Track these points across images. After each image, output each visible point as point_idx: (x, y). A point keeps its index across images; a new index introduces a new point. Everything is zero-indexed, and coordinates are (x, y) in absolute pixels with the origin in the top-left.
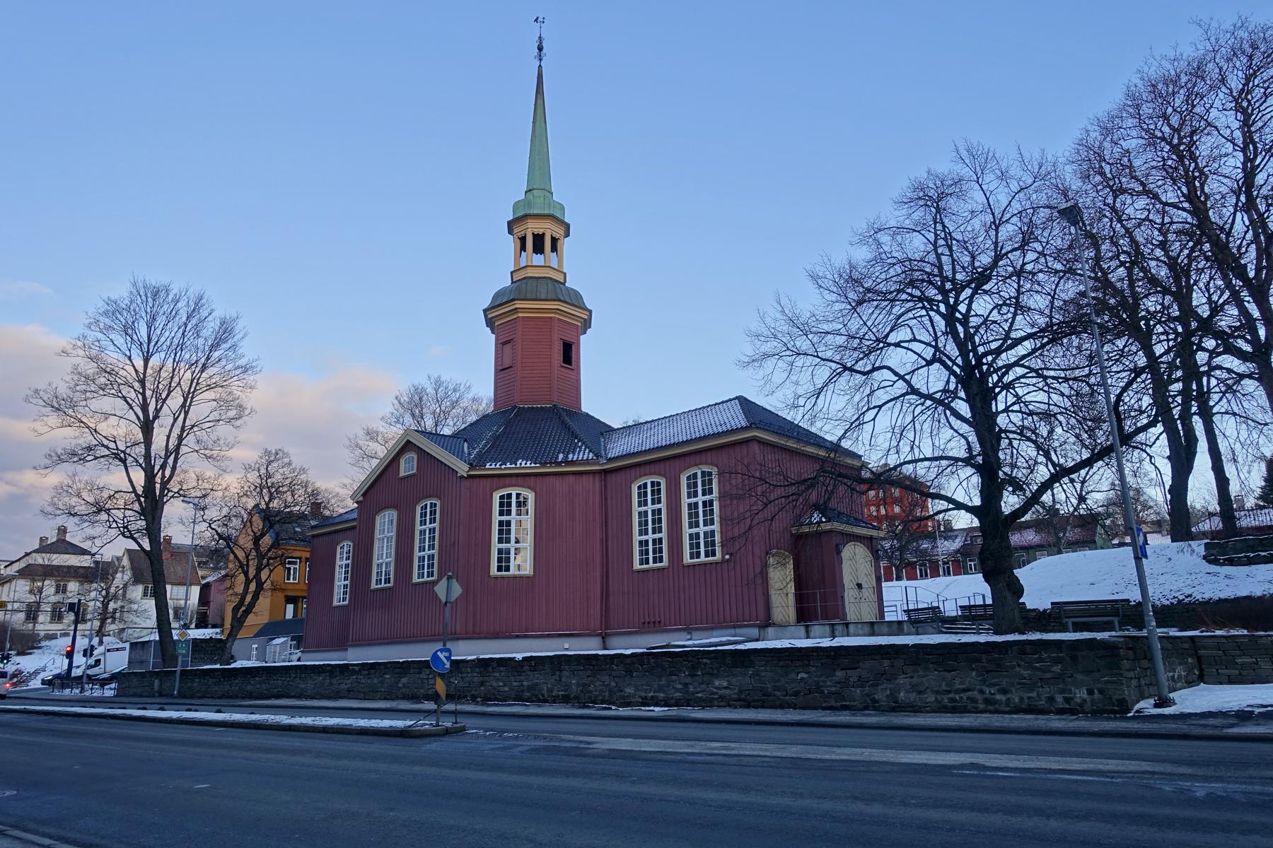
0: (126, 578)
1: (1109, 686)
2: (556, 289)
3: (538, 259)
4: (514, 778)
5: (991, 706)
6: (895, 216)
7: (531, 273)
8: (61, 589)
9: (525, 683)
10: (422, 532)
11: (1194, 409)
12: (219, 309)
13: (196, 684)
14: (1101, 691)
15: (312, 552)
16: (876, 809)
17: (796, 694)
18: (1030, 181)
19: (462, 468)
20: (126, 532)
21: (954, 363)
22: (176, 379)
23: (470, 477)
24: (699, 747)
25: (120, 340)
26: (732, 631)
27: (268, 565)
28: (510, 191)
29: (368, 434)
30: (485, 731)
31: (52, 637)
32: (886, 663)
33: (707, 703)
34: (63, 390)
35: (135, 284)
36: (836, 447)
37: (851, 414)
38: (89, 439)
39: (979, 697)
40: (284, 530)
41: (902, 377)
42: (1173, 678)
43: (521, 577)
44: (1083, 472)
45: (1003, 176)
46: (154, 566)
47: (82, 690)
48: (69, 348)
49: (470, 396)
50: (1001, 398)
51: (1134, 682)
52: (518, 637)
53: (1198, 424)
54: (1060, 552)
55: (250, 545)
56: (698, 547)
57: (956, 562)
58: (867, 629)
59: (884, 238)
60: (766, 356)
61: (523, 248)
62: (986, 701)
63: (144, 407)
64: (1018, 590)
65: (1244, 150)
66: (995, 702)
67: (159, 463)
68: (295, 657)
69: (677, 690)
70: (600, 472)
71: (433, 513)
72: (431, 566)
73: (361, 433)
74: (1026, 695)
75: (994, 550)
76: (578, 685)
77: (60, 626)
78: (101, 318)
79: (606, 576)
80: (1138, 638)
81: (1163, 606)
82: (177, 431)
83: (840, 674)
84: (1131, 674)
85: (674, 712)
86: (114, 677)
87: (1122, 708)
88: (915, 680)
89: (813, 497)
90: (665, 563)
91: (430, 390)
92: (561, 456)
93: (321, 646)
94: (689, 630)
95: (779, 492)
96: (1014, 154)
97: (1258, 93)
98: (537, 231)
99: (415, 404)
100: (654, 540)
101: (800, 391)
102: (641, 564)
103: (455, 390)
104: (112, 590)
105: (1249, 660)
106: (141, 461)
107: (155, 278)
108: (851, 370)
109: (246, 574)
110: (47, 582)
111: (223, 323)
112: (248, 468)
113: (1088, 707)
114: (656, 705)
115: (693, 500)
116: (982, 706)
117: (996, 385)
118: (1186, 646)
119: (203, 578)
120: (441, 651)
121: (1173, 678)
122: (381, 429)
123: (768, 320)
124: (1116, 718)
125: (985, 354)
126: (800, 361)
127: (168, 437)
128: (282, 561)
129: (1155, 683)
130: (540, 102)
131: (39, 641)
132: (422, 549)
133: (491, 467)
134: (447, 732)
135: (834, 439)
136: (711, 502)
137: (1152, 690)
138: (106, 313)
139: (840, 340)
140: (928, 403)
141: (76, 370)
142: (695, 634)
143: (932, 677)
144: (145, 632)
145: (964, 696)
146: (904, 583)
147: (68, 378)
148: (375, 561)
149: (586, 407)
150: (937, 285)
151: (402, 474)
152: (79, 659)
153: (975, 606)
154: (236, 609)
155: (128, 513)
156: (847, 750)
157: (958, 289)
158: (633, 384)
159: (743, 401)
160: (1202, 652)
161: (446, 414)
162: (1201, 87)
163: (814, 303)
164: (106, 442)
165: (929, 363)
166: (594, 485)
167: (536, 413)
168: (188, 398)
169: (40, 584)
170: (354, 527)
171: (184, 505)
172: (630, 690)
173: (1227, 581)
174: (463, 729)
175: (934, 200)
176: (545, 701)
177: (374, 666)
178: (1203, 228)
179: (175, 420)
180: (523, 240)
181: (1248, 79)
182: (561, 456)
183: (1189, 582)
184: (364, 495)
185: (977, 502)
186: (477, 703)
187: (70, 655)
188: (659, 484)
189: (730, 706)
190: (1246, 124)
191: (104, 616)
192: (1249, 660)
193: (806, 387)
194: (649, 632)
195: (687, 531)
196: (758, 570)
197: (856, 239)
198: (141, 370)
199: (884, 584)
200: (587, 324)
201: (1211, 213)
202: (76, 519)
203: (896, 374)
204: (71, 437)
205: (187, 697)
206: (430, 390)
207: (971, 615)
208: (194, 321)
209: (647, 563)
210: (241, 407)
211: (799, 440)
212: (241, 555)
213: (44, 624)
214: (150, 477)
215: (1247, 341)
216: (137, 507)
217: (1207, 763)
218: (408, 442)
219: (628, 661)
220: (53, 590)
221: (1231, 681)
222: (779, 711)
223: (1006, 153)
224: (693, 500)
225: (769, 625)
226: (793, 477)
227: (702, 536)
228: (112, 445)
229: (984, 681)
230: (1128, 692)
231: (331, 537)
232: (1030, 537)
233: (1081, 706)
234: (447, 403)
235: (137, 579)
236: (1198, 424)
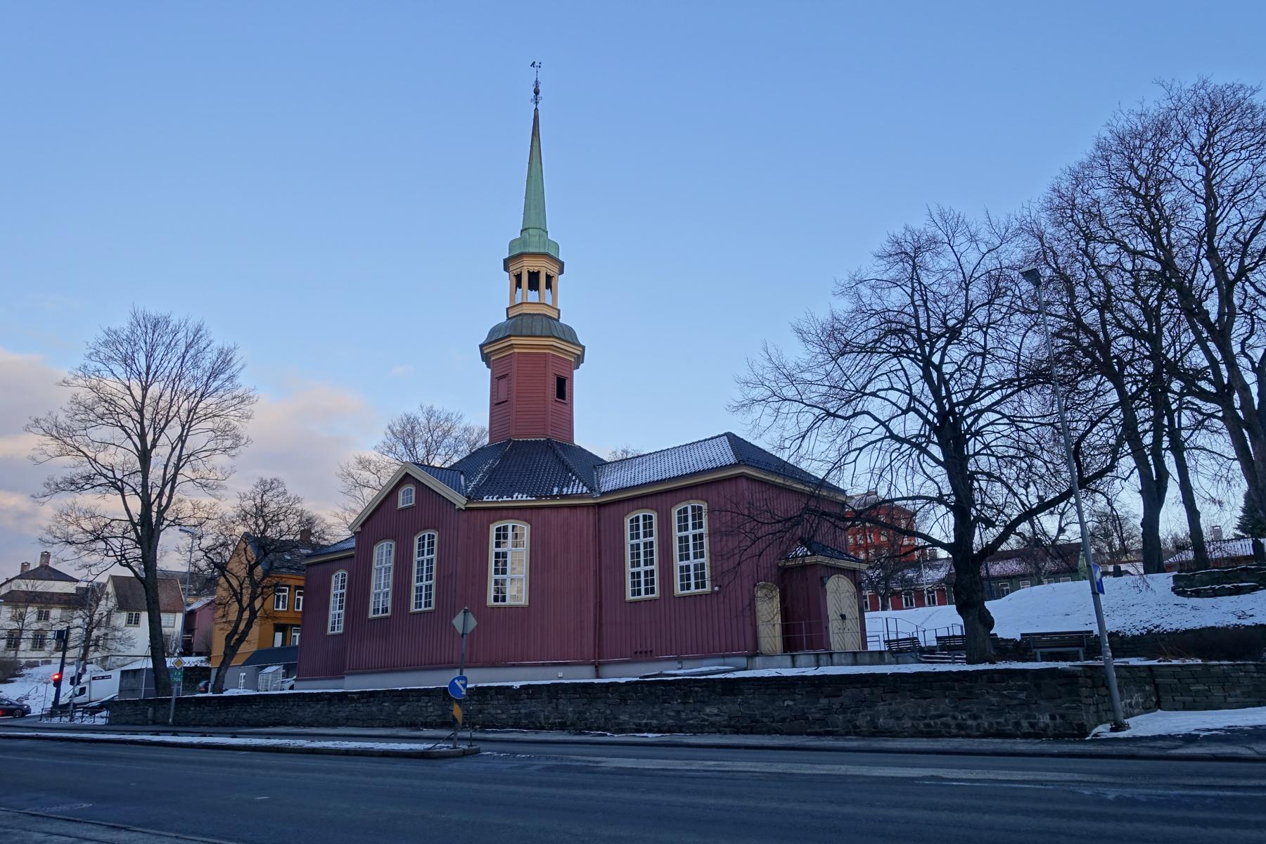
0: (111, 605)
1: (1071, 712)
2: (549, 325)
3: (533, 296)
4: (537, 790)
5: (963, 731)
6: (875, 269)
7: (527, 310)
8: (44, 616)
9: (523, 711)
10: (421, 563)
11: (1165, 445)
12: (218, 339)
13: (192, 712)
14: (1062, 717)
15: (306, 580)
16: (847, 809)
17: (783, 720)
18: (997, 242)
19: (460, 501)
20: (123, 561)
21: (929, 410)
22: (175, 409)
23: (468, 509)
24: (696, 765)
25: (119, 370)
26: (721, 661)
27: (262, 593)
28: (507, 229)
29: (360, 462)
30: (500, 752)
31: (33, 665)
32: (867, 691)
33: (698, 729)
34: (63, 419)
35: (134, 316)
36: (822, 483)
37: (833, 455)
38: (87, 469)
39: (953, 723)
40: (275, 559)
41: (882, 423)
42: (1130, 704)
43: (517, 607)
44: (1062, 505)
45: (973, 239)
46: (144, 591)
47: (72, 719)
48: (70, 378)
49: (462, 426)
50: (971, 442)
51: (1092, 709)
52: (513, 666)
53: (1170, 461)
54: (1040, 583)
55: (243, 574)
56: (688, 579)
57: (941, 591)
58: (850, 659)
59: (865, 291)
60: (754, 401)
61: (519, 285)
62: (959, 726)
63: (142, 436)
64: (988, 622)
65: (1206, 202)
66: (967, 727)
67: (156, 491)
68: (287, 685)
70: (593, 505)
71: (431, 544)
72: (428, 596)
73: (353, 462)
74: (994, 721)
75: (970, 583)
76: (574, 711)
77: (42, 654)
78: (102, 349)
79: (599, 606)
80: (1097, 667)
81: (1133, 636)
82: (174, 459)
83: (824, 701)
84: (1090, 701)
85: (667, 737)
86: (104, 706)
87: (1080, 732)
88: (894, 707)
89: (799, 532)
90: (656, 595)
91: (423, 420)
92: (556, 490)
93: (313, 675)
94: (679, 660)
95: (766, 529)
96: (982, 218)
97: (1217, 150)
98: (532, 269)
99: (406, 434)
100: (646, 572)
101: (786, 435)
102: (633, 595)
103: (447, 420)
104: (96, 617)
105: (1201, 687)
106: (139, 490)
107: (155, 309)
108: (835, 415)
109: (240, 602)
110: (30, 609)
111: (221, 353)
112: (243, 497)
113: (1050, 731)
114: (650, 731)
115: (684, 534)
116: (954, 731)
118: (1144, 674)
119: (189, 605)
120: (459, 679)
121: (1130, 704)
122: (373, 458)
123: (756, 368)
124: (1075, 742)
125: (958, 404)
126: (786, 407)
127: (166, 467)
128: (277, 588)
129: (1112, 710)
130: (536, 144)
131: (21, 669)
132: (420, 579)
133: (489, 500)
134: (464, 754)
135: (821, 475)
136: (701, 536)
137: (1110, 715)
138: (106, 344)
139: (824, 389)
140: (906, 446)
141: (75, 400)
142: (686, 663)
143: (908, 705)
144: (129, 659)
145: (939, 721)
146: (890, 613)
147: (67, 407)
148: (373, 590)
149: (577, 442)
150: (914, 336)
151: (400, 505)
152: (67, 688)
153: (954, 636)
154: (229, 638)
155: (126, 541)
156: (826, 767)
157: (934, 338)
158: (626, 418)
159: (731, 437)
160: (1158, 680)
161: (438, 444)
162: (1164, 142)
163: (797, 354)
164: (105, 471)
165: (905, 412)
166: (588, 518)
167: (530, 446)
168: (186, 427)
169: (23, 610)
170: (351, 557)
171: (183, 534)
172: (624, 718)
173: (1194, 612)
174: (478, 751)
175: (910, 255)
176: (542, 728)
177: (372, 694)
178: (1170, 276)
179: (173, 449)
180: (519, 278)
181: (1210, 134)
182: (556, 490)
183: (1158, 613)
184: (362, 526)
186: (475, 730)
187: (57, 683)
188: (651, 518)
189: (720, 732)
190: (1207, 180)
191: (88, 643)
192: (1201, 687)
193: (792, 430)
194: (641, 662)
195: (678, 564)
196: (746, 602)
197: (839, 290)
198: (139, 399)
199: (866, 615)
200: (580, 359)
201: (1176, 260)
202: (73, 548)
203: (875, 419)
204: (70, 466)
205: (181, 725)
206: (423, 420)
207: (946, 646)
208: (192, 352)
209: (639, 594)
210: (238, 437)
211: (785, 476)
212: (235, 583)
213: (25, 652)
214: (147, 505)
215: (1210, 381)
216: (133, 536)
217: (1119, 775)
218: (407, 474)
219: (623, 689)
220: (35, 617)
221: (1187, 707)
222: (766, 737)
223: (976, 220)
224: (684, 534)
225: (756, 655)
226: (780, 514)
227: (692, 568)
228: (110, 474)
230: (1086, 717)
231: (327, 566)
232: (1013, 567)
233: (1045, 730)
234: (438, 433)
235: (122, 606)
236: (1170, 461)
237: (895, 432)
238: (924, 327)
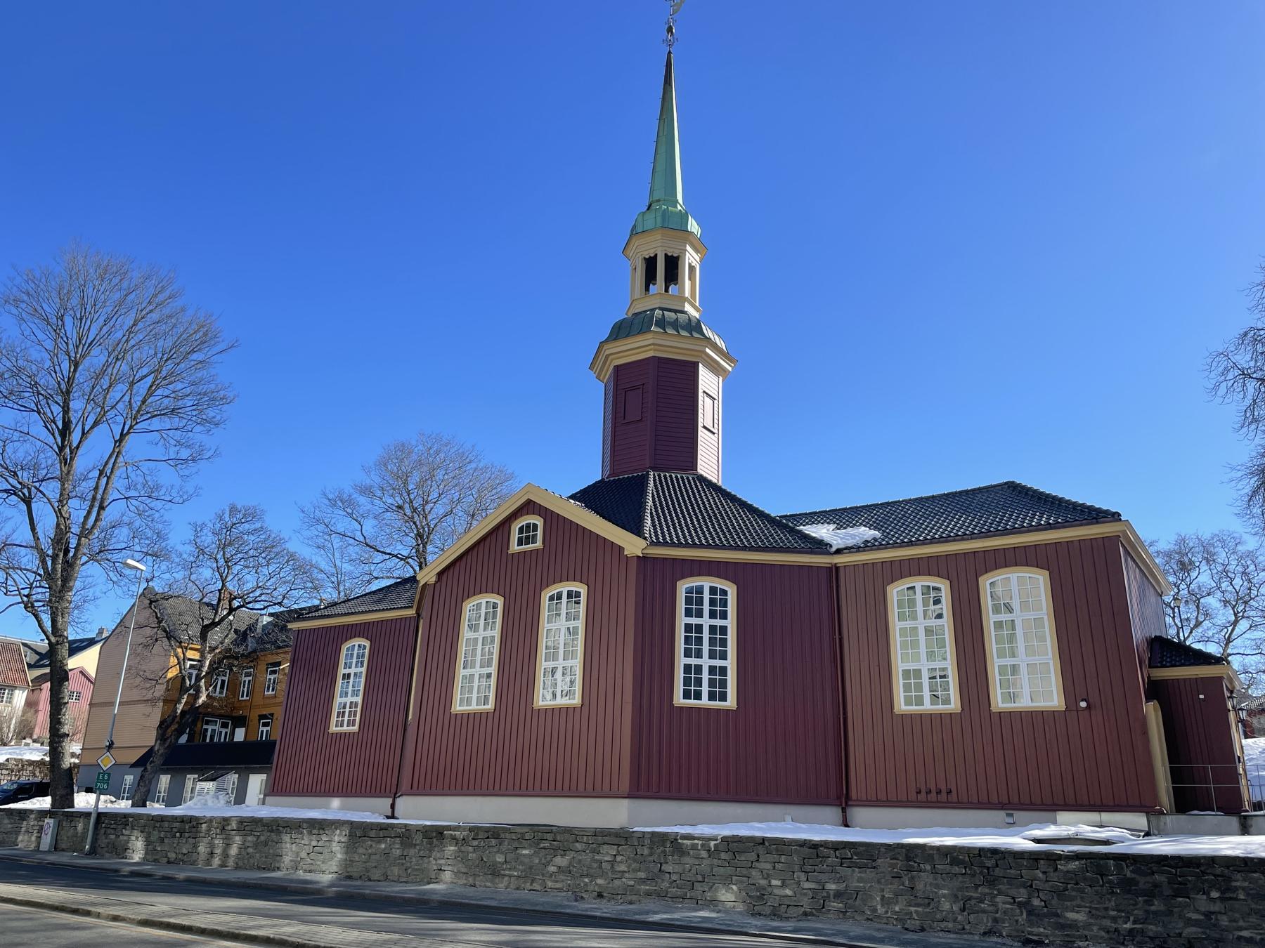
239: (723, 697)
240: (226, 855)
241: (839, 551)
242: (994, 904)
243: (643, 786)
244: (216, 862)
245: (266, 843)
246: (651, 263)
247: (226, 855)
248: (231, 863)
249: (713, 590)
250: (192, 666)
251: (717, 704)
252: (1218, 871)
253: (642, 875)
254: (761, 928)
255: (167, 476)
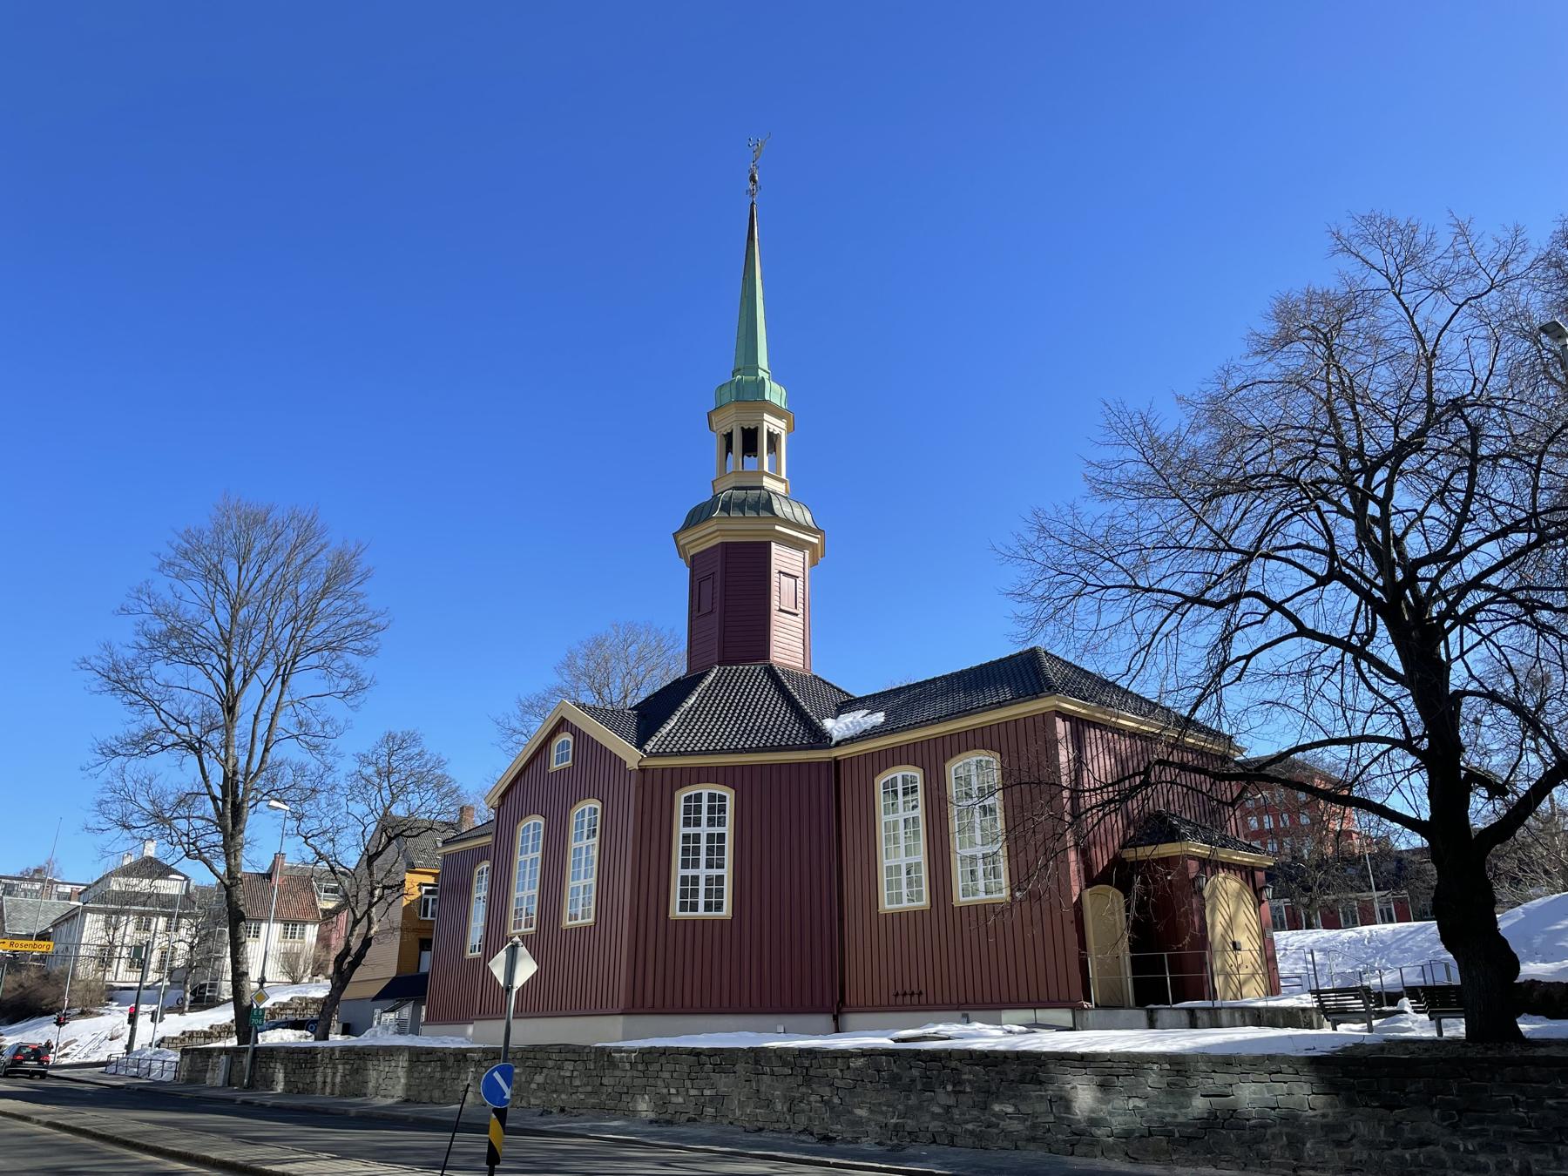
9: (707, 1092)
50: (1453, 636)
61: (729, 448)
69: (935, 1116)
117: (1443, 616)
165: (1322, 582)
180: (729, 437)
184: (503, 796)
185: (1426, 815)
229: (1455, 1128)
237: (1309, 625)
238: (1352, 444)
239: (719, 907)
240: (334, 1084)
241: (838, 744)
242: (809, 1103)
243: (638, 1005)
244: (328, 1090)
245: (357, 1071)
246: (729, 437)
247: (334, 1084)
248: (337, 1092)
249: (712, 797)
250: (428, 892)
251: (713, 914)
252: (954, 1064)
253: (589, 1089)
254: (592, 1129)
255: (335, 709)
